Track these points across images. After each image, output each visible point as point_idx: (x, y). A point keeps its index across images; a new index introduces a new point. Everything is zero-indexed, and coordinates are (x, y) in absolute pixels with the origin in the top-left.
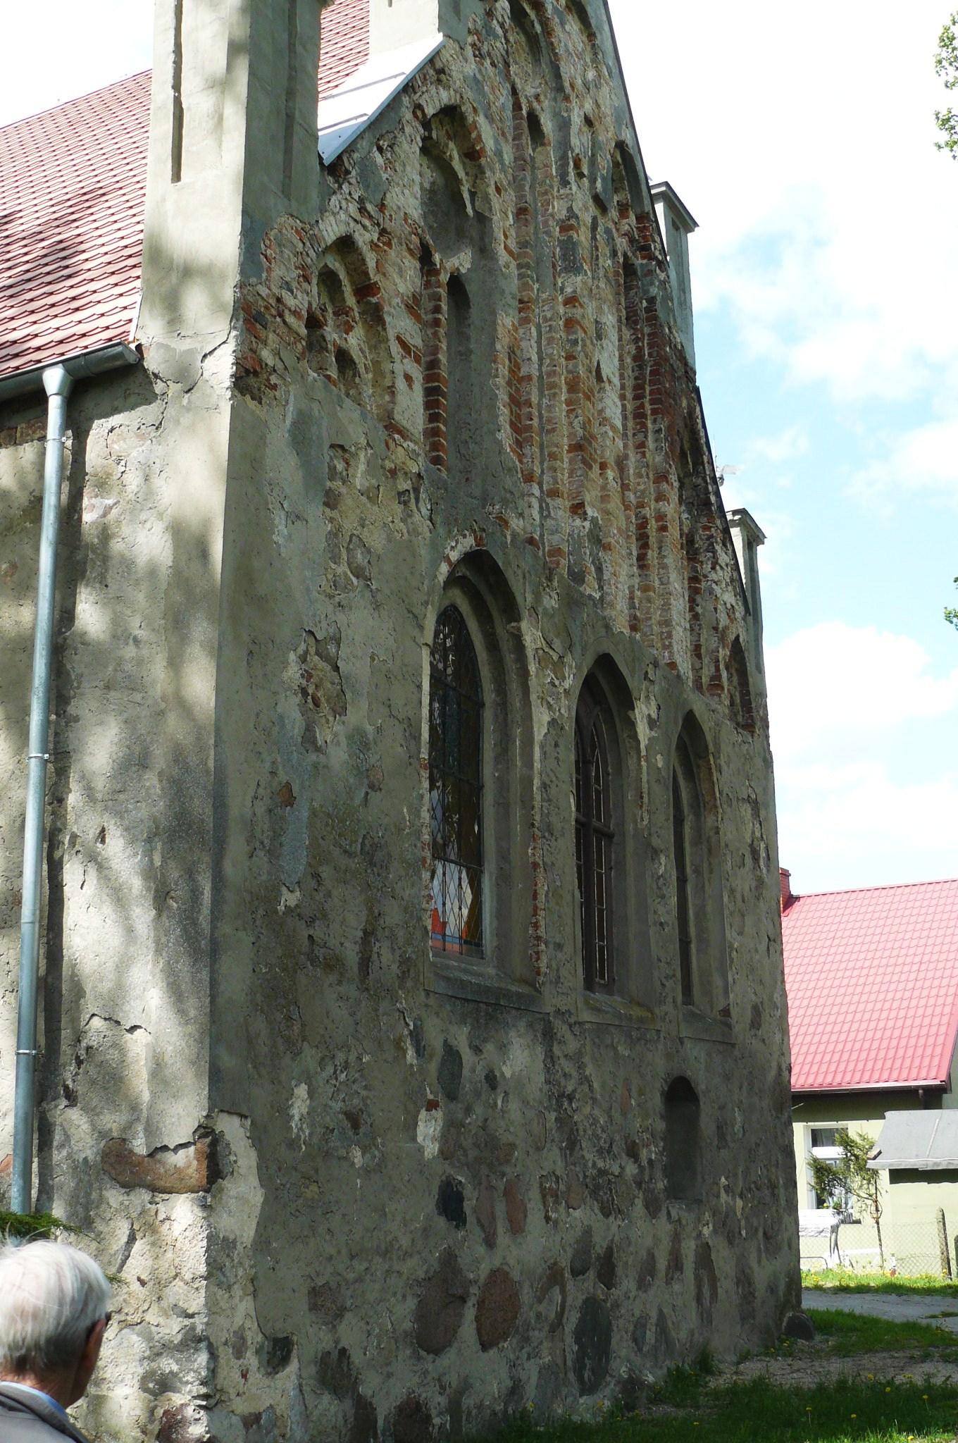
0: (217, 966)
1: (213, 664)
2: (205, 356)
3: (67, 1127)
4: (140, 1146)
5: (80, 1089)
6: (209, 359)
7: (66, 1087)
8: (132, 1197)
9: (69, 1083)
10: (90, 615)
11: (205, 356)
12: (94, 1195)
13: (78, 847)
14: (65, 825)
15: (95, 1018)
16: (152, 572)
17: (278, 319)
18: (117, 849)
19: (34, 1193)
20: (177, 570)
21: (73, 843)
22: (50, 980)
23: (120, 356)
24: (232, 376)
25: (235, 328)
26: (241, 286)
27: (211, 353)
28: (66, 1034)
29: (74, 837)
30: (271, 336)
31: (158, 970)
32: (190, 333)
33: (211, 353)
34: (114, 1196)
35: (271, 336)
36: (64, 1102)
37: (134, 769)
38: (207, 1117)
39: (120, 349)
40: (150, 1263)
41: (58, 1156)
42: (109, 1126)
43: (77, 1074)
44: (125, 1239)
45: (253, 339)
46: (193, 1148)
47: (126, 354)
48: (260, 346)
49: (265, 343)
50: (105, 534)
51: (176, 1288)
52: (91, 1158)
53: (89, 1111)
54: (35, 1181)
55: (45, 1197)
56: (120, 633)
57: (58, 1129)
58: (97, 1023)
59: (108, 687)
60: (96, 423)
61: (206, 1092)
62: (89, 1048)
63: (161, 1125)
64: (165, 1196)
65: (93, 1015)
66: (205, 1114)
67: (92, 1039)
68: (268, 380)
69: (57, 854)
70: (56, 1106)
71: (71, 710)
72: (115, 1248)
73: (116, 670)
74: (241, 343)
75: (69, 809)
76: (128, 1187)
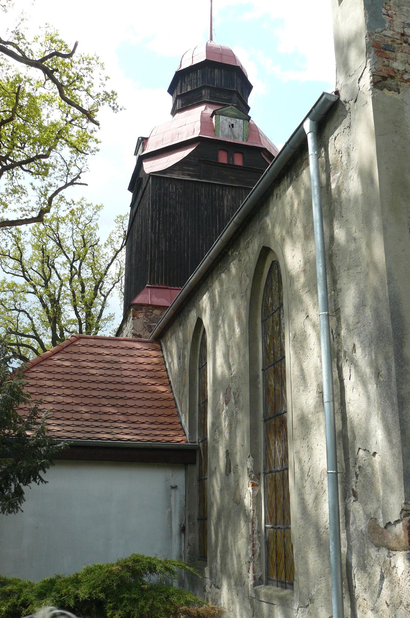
0: (405, 412)
1: (382, 238)
2: (359, 80)
3: (354, 512)
4: (381, 522)
5: (358, 491)
6: (362, 80)
7: (353, 490)
8: (380, 553)
9: (354, 487)
10: (340, 234)
11: (359, 80)
12: (366, 552)
13: (347, 358)
14: (341, 347)
15: (361, 450)
16: (356, 201)
17: (404, 45)
18: (359, 354)
19: (344, 550)
20: (364, 195)
21: (345, 356)
22: (343, 432)
23: (326, 101)
24: (371, 82)
25: (369, 58)
26: (369, 35)
27: (361, 77)
28: (351, 460)
29: (345, 352)
30: (399, 55)
31: (379, 419)
32: (353, 73)
33: (361, 77)
34: (373, 551)
35: (399, 55)
36: (353, 498)
37: (361, 308)
38: (405, 503)
39: (324, 97)
40: (390, 592)
41: (352, 528)
42: (370, 511)
43: (356, 482)
44: (379, 578)
45: (385, 60)
46: (401, 524)
47: (329, 98)
48: (391, 61)
49: (395, 59)
50: (339, 190)
51: (401, 610)
52: (364, 530)
53: (364, 504)
54: (197, 414)
55: (349, 551)
56: (351, 238)
57: (351, 513)
58: (361, 453)
59: (348, 269)
60: (330, 138)
61: (403, 489)
62: (359, 467)
63: (387, 509)
64: (394, 553)
65: (359, 449)
66: (403, 502)
67: (360, 462)
68: (402, 78)
69: (340, 363)
70: (350, 501)
71: (338, 286)
72: (376, 583)
73: (350, 259)
74: (374, 64)
75: (342, 338)
76: (378, 547)
